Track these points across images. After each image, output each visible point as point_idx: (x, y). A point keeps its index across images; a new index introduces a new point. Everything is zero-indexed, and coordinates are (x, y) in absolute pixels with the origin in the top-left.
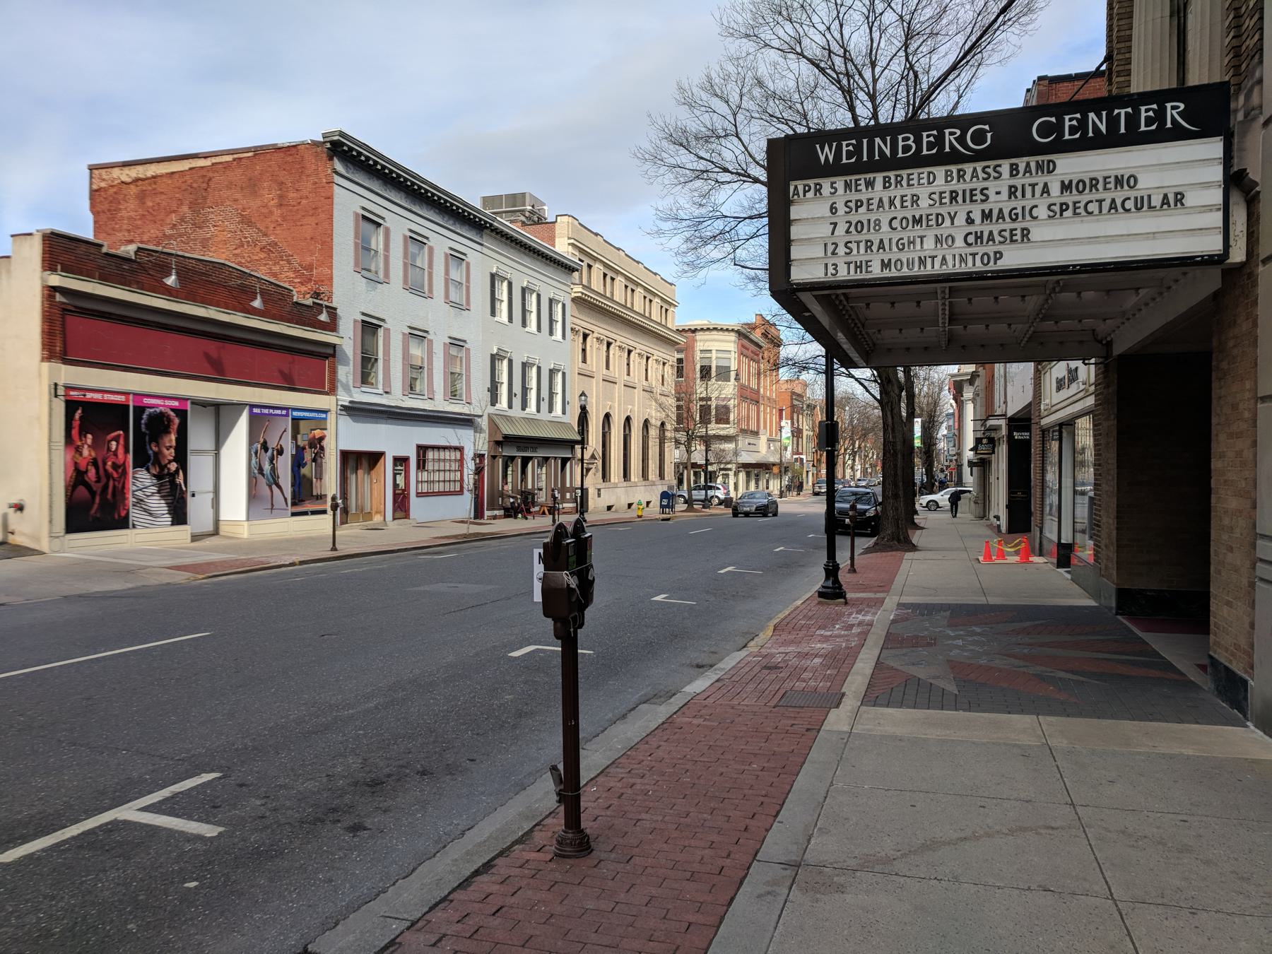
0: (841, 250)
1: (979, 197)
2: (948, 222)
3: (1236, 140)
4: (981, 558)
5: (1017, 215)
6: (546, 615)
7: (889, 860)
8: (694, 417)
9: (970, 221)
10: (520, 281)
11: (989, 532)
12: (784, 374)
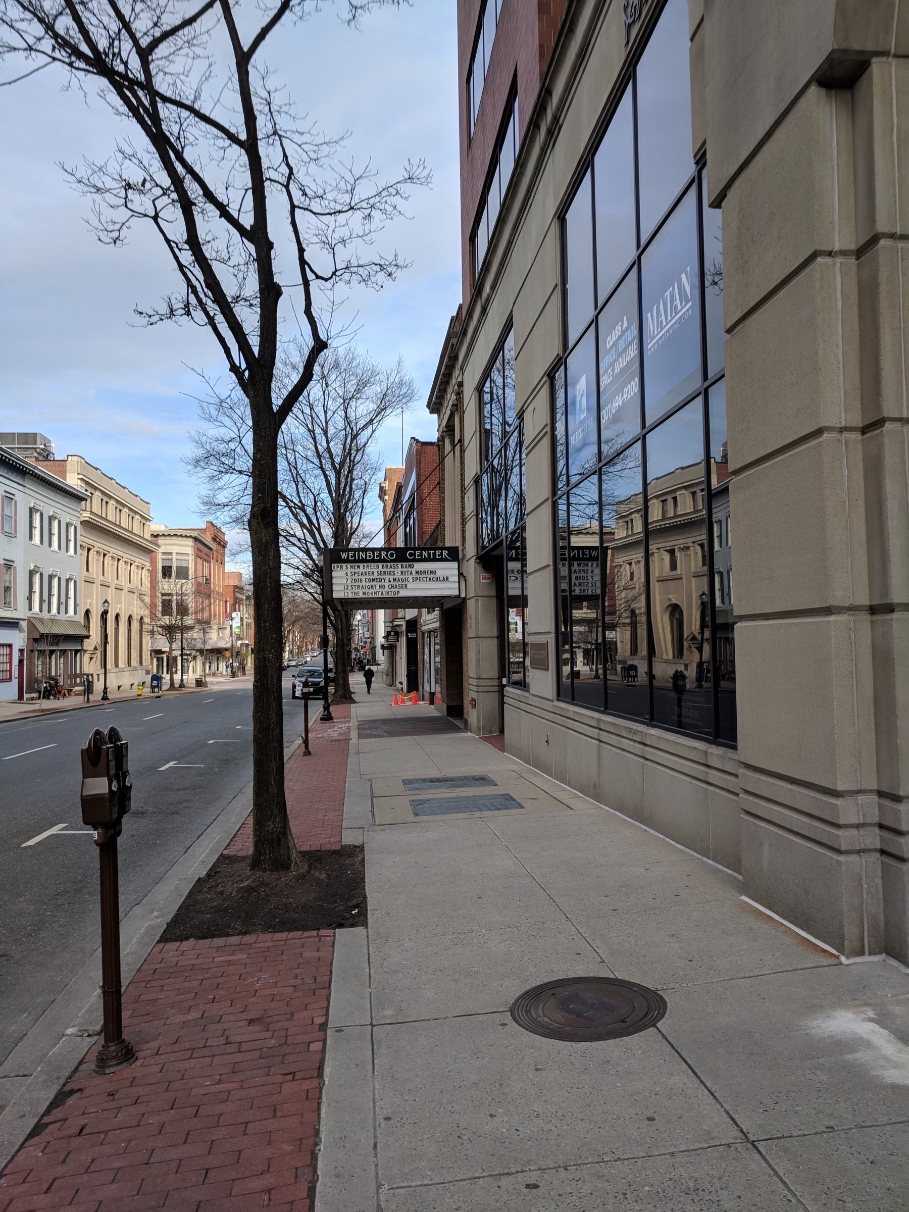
0: (350, 588)
8: (173, 617)
10: (48, 511)
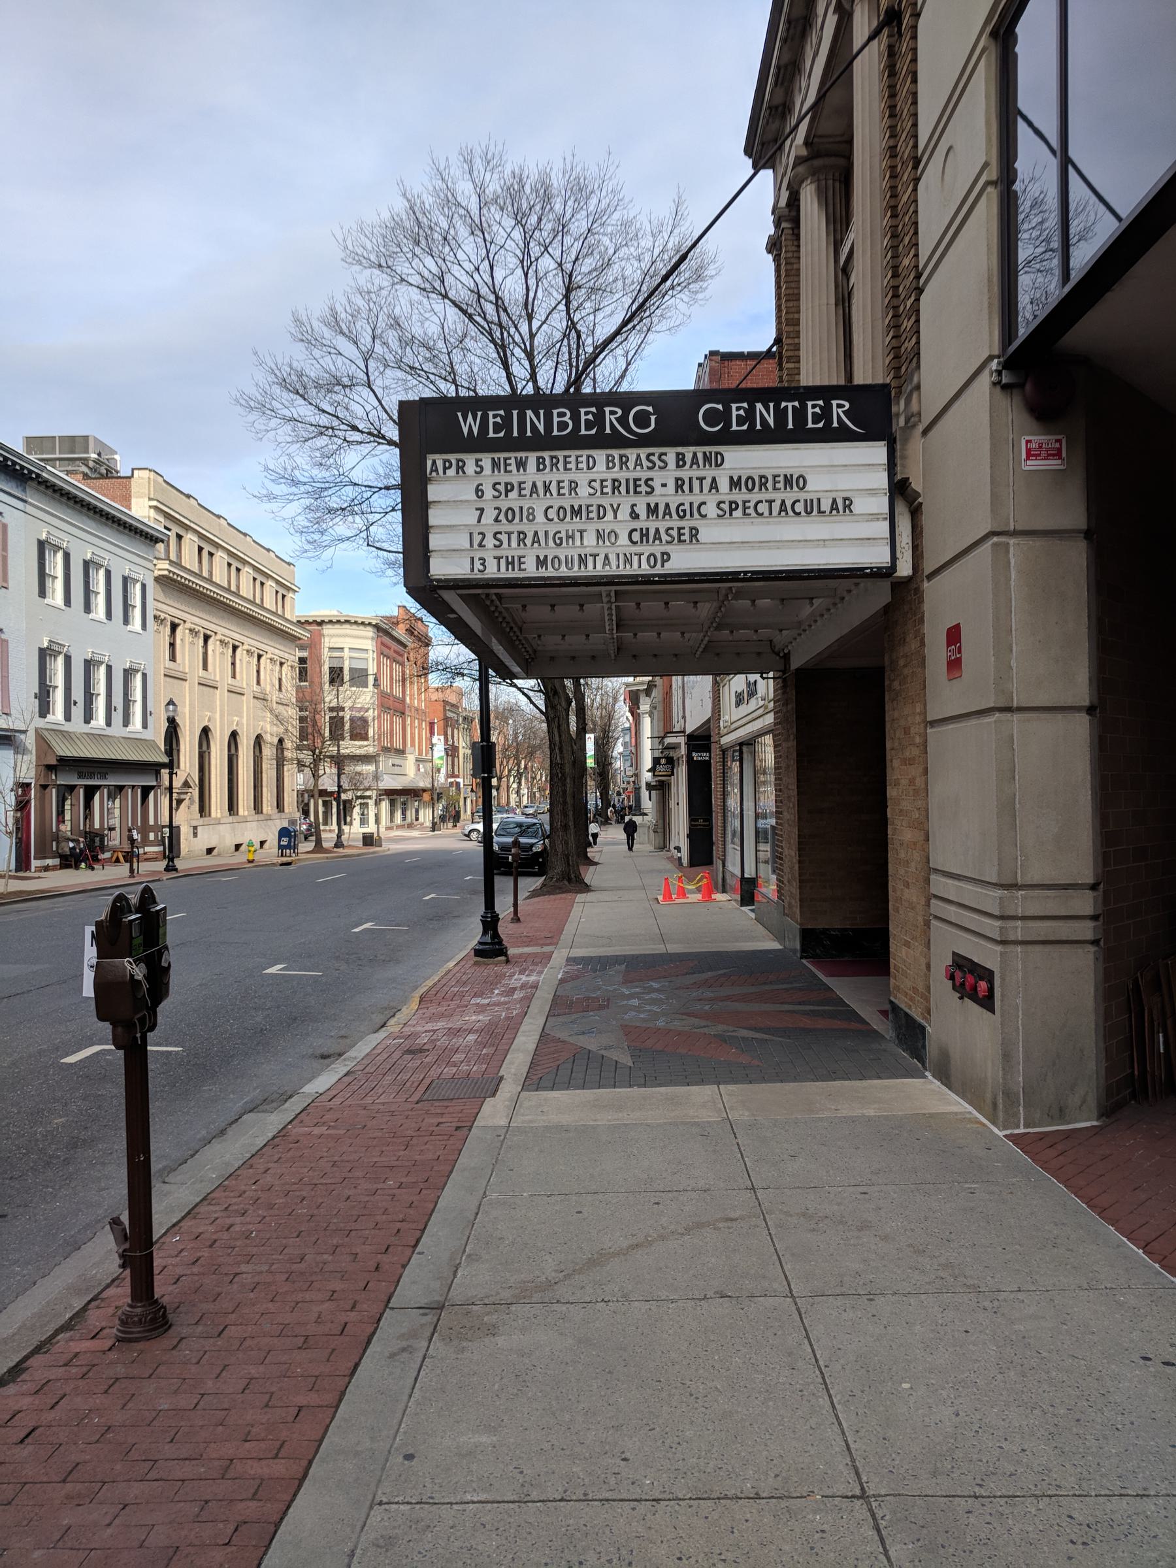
0: (490, 542)
1: (643, 488)
2: (610, 516)
3: (898, 446)
4: (660, 898)
5: (684, 511)
6: (101, 1018)
7: (550, 1285)
8: (321, 733)
9: (634, 516)
10: (82, 551)
11: (669, 866)
12: (434, 680)
